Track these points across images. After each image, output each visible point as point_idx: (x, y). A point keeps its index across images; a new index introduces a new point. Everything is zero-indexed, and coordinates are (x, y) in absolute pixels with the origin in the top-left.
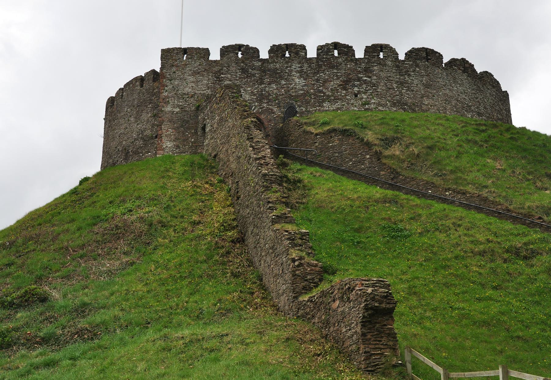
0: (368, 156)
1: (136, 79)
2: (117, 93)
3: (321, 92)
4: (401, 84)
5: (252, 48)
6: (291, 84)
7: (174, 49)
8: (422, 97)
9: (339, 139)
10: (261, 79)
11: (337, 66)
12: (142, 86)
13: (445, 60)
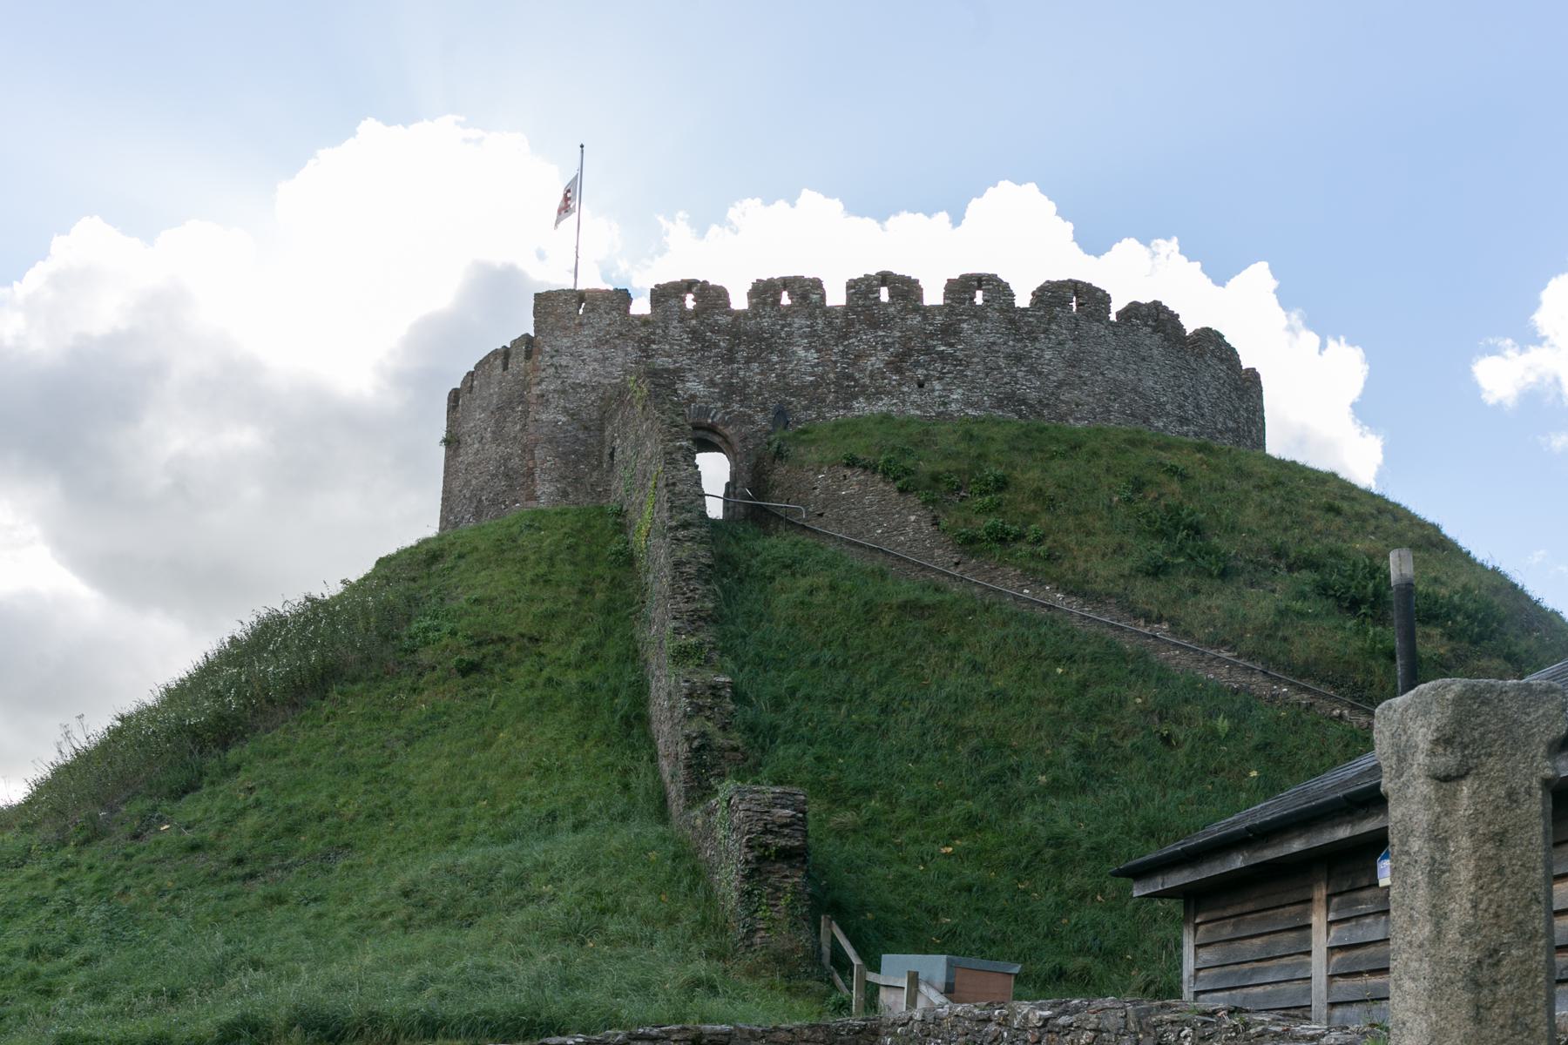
0: (913, 518)
1: (495, 353)
2: (464, 382)
3: (850, 377)
4: (1018, 359)
7: (559, 293)
9: (859, 483)
10: (730, 350)
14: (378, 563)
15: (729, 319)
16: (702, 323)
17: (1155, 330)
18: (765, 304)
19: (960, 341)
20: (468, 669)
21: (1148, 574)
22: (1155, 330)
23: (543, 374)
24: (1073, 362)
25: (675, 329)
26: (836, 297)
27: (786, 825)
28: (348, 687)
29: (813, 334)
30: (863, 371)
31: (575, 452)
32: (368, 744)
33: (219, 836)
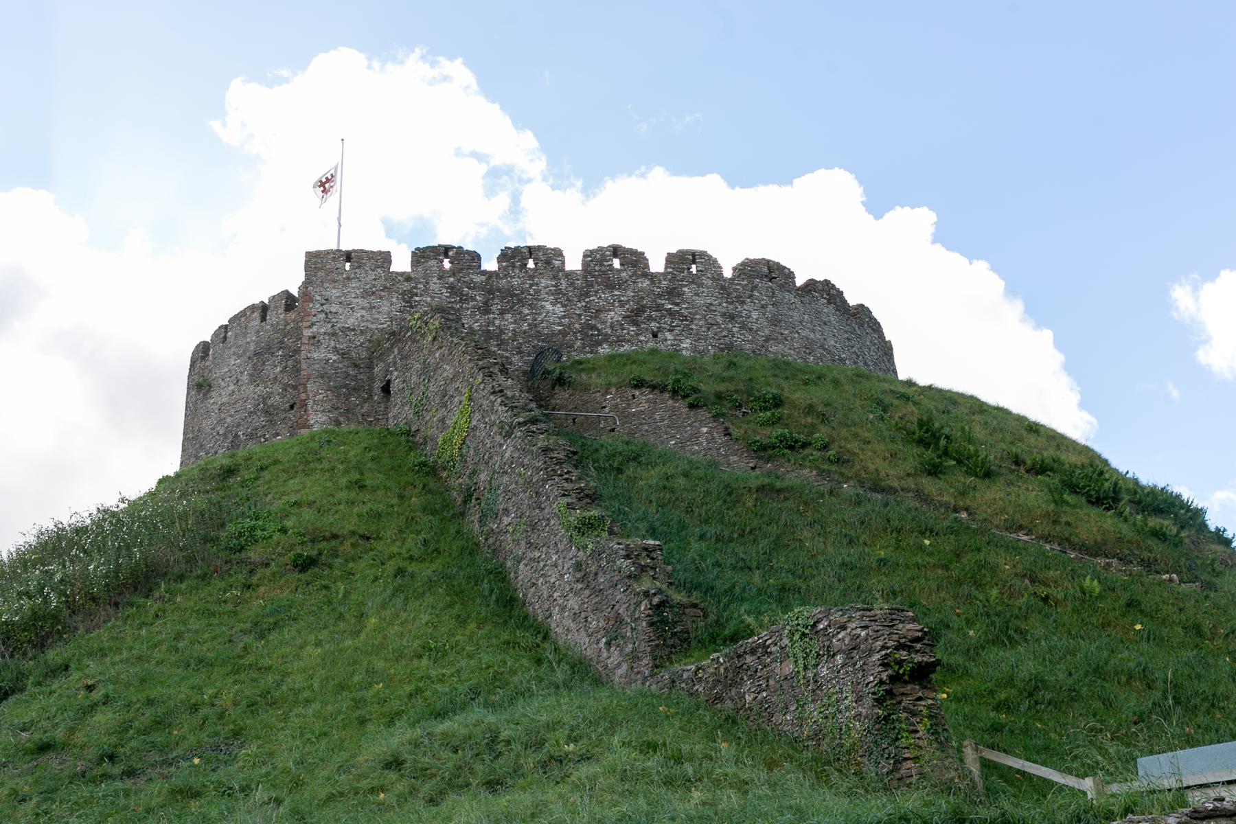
0: (705, 430)
1: (252, 308)
2: (216, 334)
3: (593, 327)
4: (732, 317)
5: (468, 252)
6: (540, 314)
7: (328, 252)
8: (767, 341)
9: (648, 401)
10: (486, 303)
11: (621, 285)
12: (263, 319)
13: (800, 282)
14: (160, 482)
15: (483, 278)
16: (459, 281)
17: (829, 302)
18: (514, 267)
19: (684, 302)
20: (305, 565)
21: (930, 474)
22: (829, 302)
23: (315, 319)
24: (775, 322)
25: (435, 284)
26: (573, 263)
27: (917, 640)
28: (173, 586)
29: (558, 292)
30: (604, 323)
31: (346, 386)
32: (214, 638)
33: (72, 731)
